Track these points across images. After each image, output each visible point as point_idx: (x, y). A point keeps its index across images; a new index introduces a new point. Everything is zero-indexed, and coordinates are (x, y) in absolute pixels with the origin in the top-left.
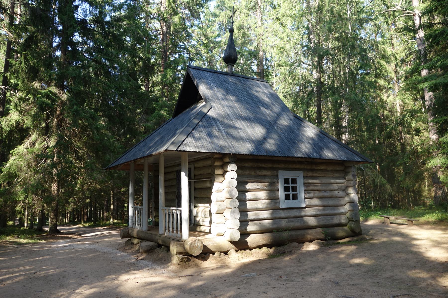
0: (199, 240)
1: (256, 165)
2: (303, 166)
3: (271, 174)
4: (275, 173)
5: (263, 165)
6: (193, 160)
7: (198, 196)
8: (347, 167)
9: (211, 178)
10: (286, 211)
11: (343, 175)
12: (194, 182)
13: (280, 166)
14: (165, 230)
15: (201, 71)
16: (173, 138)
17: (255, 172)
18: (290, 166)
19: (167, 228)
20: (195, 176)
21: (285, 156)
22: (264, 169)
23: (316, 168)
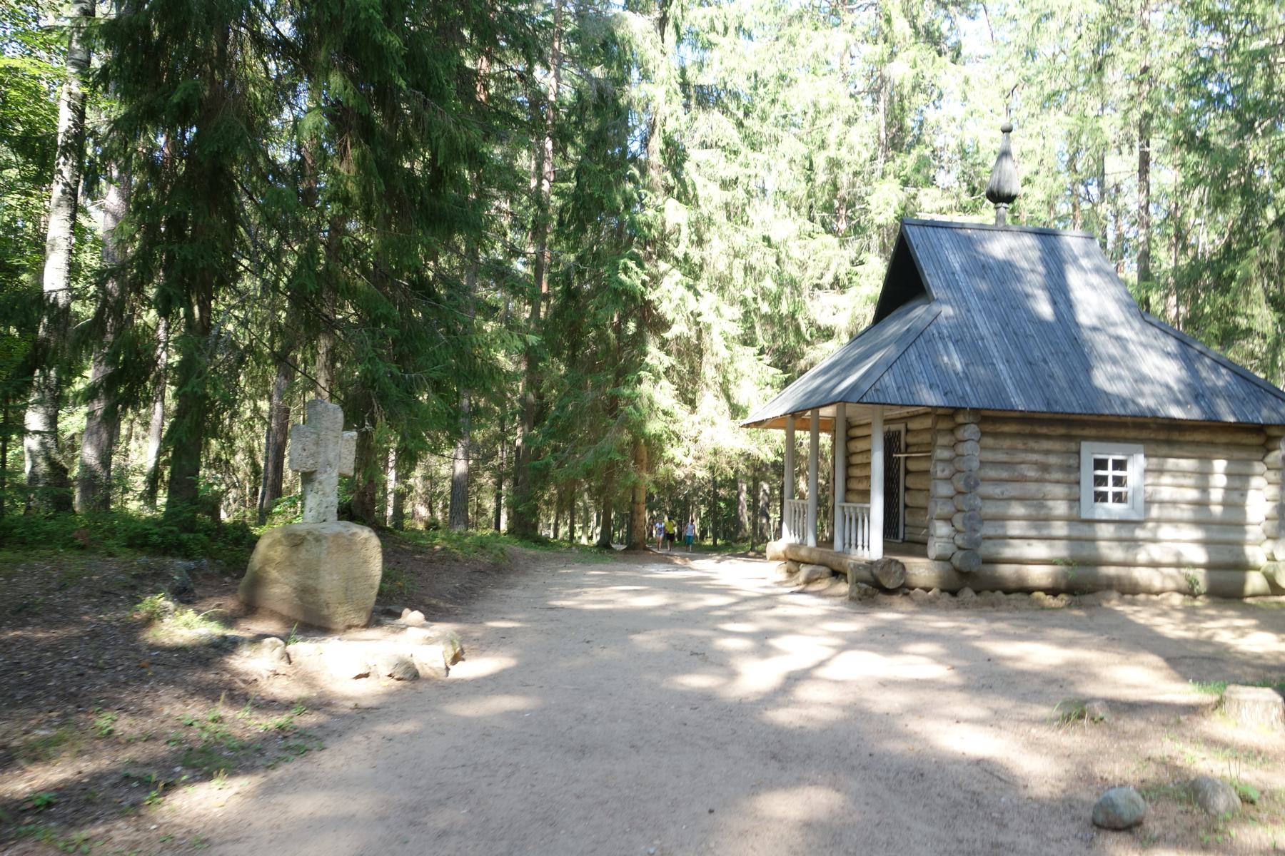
0: (897, 562)
1: (1027, 429)
2: (1145, 434)
3: (1065, 449)
4: (1073, 446)
5: (1044, 430)
6: (906, 415)
7: (911, 486)
8: (1270, 439)
9: (929, 452)
10: (1219, 546)
11: (1260, 456)
12: (906, 458)
13: (1086, 432)
14: (844, 545)
15: (930, 229)
16: (847, 388)
17: (1024, 444)
18: (1112, 433)
19: (847, 541)
20: (907, 446)
21: (1090, 412)
22: (1047, 437)
23: (1181, 438)
